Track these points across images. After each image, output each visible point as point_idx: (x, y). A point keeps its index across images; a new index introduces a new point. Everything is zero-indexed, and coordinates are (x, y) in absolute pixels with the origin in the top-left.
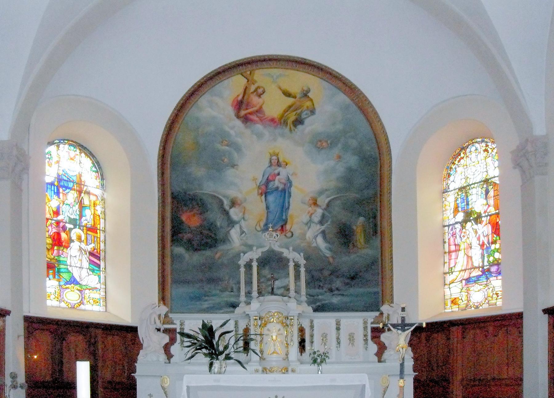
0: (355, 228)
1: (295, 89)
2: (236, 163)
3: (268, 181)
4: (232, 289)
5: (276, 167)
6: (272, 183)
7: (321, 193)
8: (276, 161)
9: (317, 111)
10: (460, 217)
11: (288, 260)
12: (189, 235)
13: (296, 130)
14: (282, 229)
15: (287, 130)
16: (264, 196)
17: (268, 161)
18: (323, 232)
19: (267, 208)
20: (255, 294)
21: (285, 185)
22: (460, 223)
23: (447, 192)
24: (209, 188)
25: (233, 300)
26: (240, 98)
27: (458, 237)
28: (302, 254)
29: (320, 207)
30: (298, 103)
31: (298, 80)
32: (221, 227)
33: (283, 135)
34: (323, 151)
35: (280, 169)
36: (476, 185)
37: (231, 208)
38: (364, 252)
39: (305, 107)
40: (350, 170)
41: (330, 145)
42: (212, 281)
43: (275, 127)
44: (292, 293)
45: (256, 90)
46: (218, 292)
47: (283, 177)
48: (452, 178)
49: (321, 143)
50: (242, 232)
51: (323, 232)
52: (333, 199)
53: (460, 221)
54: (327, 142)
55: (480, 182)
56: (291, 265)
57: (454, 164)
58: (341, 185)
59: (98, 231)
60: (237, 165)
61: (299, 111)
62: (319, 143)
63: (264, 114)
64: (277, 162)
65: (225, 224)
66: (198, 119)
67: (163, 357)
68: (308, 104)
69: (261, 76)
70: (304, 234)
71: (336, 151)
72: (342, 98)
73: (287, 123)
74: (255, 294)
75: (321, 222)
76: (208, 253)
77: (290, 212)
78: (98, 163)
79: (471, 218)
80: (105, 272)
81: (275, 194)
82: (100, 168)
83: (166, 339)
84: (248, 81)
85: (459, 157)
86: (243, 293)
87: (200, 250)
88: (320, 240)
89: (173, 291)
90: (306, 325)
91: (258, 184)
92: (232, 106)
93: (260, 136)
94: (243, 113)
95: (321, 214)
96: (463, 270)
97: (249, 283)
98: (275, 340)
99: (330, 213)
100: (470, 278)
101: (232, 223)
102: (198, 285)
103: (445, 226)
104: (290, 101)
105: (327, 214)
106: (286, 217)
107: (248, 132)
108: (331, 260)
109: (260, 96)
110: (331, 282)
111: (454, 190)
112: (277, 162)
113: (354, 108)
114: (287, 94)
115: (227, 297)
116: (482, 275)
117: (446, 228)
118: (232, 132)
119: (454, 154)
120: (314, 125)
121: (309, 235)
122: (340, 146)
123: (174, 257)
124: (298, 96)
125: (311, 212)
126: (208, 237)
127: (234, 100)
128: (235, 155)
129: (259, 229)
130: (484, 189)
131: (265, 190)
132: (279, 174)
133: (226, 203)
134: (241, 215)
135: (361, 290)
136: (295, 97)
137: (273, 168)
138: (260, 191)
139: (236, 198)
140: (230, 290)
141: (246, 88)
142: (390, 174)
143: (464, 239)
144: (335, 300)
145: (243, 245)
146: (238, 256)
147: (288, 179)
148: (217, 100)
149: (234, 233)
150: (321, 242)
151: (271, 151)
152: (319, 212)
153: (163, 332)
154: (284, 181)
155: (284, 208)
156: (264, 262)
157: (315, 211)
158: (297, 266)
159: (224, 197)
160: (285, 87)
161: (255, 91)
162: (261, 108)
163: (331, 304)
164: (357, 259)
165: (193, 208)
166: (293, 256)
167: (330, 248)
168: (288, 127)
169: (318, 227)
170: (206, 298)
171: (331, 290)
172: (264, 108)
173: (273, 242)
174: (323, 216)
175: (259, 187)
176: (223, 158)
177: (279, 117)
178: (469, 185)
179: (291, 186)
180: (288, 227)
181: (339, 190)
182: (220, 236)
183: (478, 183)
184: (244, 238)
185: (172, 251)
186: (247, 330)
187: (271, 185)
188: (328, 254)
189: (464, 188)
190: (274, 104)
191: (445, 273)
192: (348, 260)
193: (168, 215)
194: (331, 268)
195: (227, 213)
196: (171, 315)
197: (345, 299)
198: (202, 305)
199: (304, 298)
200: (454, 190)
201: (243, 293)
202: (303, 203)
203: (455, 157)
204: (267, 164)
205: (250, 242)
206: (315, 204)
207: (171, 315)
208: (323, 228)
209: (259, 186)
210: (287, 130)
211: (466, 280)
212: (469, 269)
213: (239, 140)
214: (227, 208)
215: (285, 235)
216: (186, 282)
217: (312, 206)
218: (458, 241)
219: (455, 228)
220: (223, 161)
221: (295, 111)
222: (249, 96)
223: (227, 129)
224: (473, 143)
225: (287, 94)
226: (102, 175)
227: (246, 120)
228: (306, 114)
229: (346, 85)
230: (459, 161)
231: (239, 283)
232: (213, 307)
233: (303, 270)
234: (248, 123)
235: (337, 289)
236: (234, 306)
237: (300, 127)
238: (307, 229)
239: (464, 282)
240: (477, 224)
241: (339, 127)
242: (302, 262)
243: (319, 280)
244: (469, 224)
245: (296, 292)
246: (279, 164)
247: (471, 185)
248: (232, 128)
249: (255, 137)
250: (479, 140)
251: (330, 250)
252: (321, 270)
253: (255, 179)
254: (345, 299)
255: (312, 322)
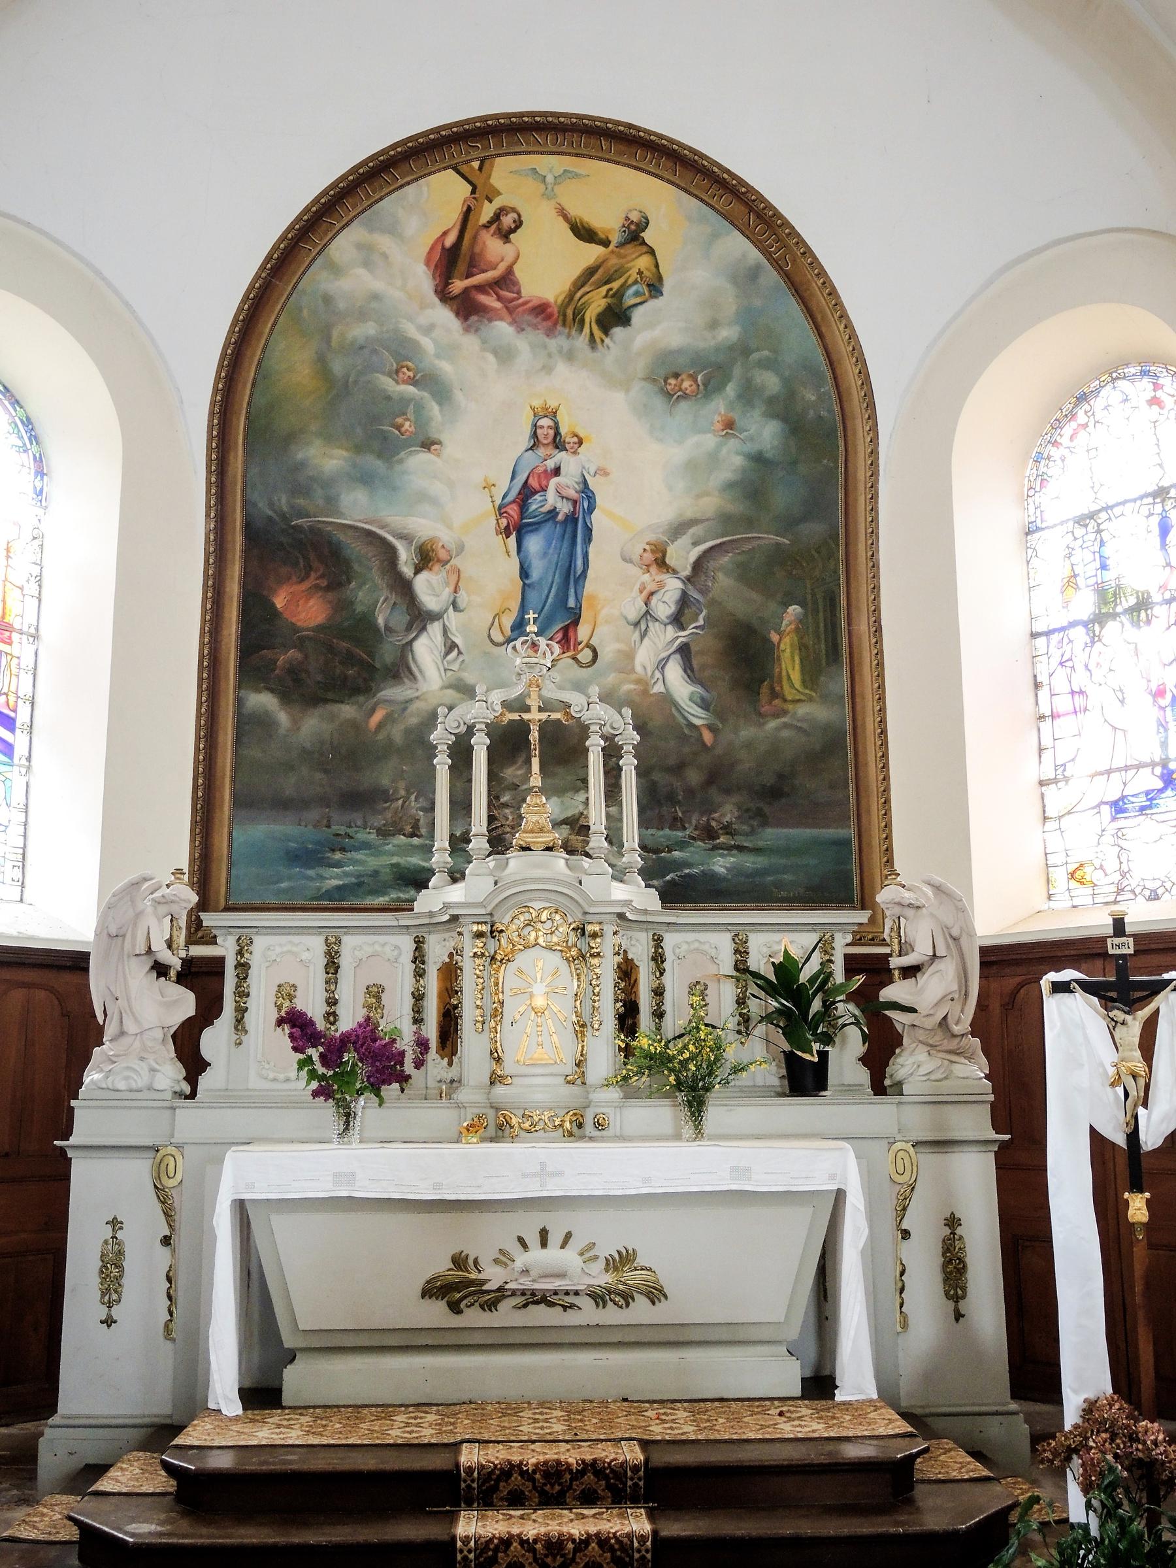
0: (775, 637)
1: (608, 221)
2: (434, 435)
3: (526, 493)
4: (416, 826)
5: (550, 450)
6: (537, 497)
7: (678, 529)
8: (552, 432)
9: (666, 289)
10: (1085, 604)
11: (584, 730)
12: (293, 654)
13: (607, 341)
14: (567, 639)
15: (582, 341)
16: (513, 537)
17: (528, 430)
18: (684, 651)
19: (524, 573)
20: (479, 844)
21: (575, 502)
22: (1085, 624)
23: (1038, 529)
24: (356, 508)
25: (415, 860)
26: (450, 241)
27: (1079, 667)
28: (627, 712)
29: (675, 572)
30: (614, 261)
31: (614, 192)
32: (387, 628)
33: (570, 356)
34: (684, 405)
35: (561, 457)
36: (1129, 506)
37: (418, 571)
38: (807, 710)
39: (633, 274)
40: (758, 459)
41: (701, 387)
42: (360, 800)
43: (550, 333)
44: (597, 842)
45: (497, 217)
46: (372, 837)
47: (568, 481)
48: (1051, 488)
49: (680, 380)
50: (451, 647)
51: (684, 651)
52: (712, 548)
53: (1085, 618)
54: (694, 378)
55: (1141, 498)
56: (595, 744)
57: (1056, 444)
58: (735, 508)
59: (15, 636)
60: (439, 443)
61: (615, 285)
62: (672, 381)
63: (519, 292)
64: (551, 437)
65: (400, 619)
66: (327, 300)
67: (171, 1073)
68: (644, 262)
69: (513, 176)
70: (630, 656)
71: (718, 407)
72: (737, 247)
73: (582, 321)
74: (479, 844)
75: (678, 620)
76: (347, 711)
77: (590, 587)
78: (28, 422)
79: (1119, 609)
80: (29, 768)
81: (547, 528)
82: (35, 438)
83: (185, 1004)
84: (473, 192)
85: (1073, 424)
86: (442, 840)
87: (326, 701)
88: (674, 672)
89: (247, 835)
90: (640, 952)
91: (498, 502)
92: (427, 263)
93: (504, 355)
94: (458, 285)
95: (677, 595)
96: (1102, 774)
97: (461, 805)
98: (540, 1012)
99: (704, 591)
100: (1123, 798)
101: (420, 618)
102: (314, 814)
103: (1034, 635)
104: (592, 253)
105: (694, 594)
106: (578, 600)
107: (470, 342)
108: (708, 737)
109: (505, 235)
110: (709, 808)
111: (1062, 523)
112: (551, 437)
113: (771, 276)
114: (584, 233)
115: (396, 853)
116: (1161, 791)
117: (1041, 642)
118: (427, 343)
119: (1058, 415)
120: (658, 327)
121: (645, 656)
122: (731, 390)
123: (251, 726)
124: (615, 239)
125: (651, 587)
126: (349, 659)
127: (432, 248)
128: (434, 409)
129: (499, 638)
130: (1155, 520)
131: (519, 517)
132: (557, 471)
133: (405, 557)
134: (447, 593)
135: (807, 833)
136: (605, 243)
137: (541, 452)
138: (504, 522)
139: (433, 540)
140: (408, 829)
141: (469, 209)
142: (875, 474)
143: (1098, 675)
144: (721, 864)
145: (450, 687)
146: (431, 720)
147: (585, 488)
148: (384, 242)
149: (426, 650)
150: (678, 685)
151: (537, 403)
152: (673, 586)
153: (178, 982)
154: (572, 494)
155: (572, 576)
156: (509, 742)
157: (661, 585)
158: (612, 752)
159: (401, 537)
160: (577, 211)
161: (491, 223)
162: (510, 271)
163: (710, 876)
164: (785, 734)
165: (309, 568)
166: (605, 720)
167: (702, 699)
168: (586, 330)
169: (671, 631)
170: (338, 856)
171: (709, 834)
172: (519, 273)
173: (536, 678)
174: (684, 601)
175: (501, 511)
176: (399, 420)
177: (560, 301)
178: (1106, 509)
179: (591, 509)
180: (583, 632)
181: (727, 521)
182: (387, 654)
183: (1135, 500)
184: (455, 667)
185: (240, 702)
186: (451, 972)
187: (535, 504)
188: (698, 716)
189: (1092, 516)
190: (546, 264)
191: (1042, 783)
192: (758, 735)
193: (233, 589)
194: (705, 759)
195: (404, 588)
196: (209, 919)
197: (750, 862)
198: (322, 878)
199: (633, 858)
200: (1062, 523)
201: (442, 840)
202: (627, 560)
203: (1057, 425)
204: (525, 441)
205: (469, 677)
206: (661, 563)
207: (209, 919)
208: (683, 636)
209: (500, 508)
210: (582, 341)
211: (1115, 803)
212: (1119, 770)
213: (445, 367)
214: (407, 570)
215: (574, 658)
216: (282, 805)
217: (654, 569)
218: (1080, 680)
219: (1071, 641)
220: (399, 427)
221: (607, 283)
222: (475, 238)
223: (412, 331)
224: (1114, 380)
225: (584, 233)
226: (39, 460)
227: (467, 308)
228: (637, 294)
229: (751, 210)
230: (1072, 438)
231: (431, 808)
232: (360, 885)
233: (629, 764)
234: (474, 318)
235: (728, 829)
236: (419, 880)
237: (618, 331)
238: (634, 651)
239: (1106, 810)
240: (1136, 624)
241: (729, 334)
242: (630, 738)
243: (671, 798)
244: (1112, 626)
245: (608, 838)
246: (558, 443)
247: (1112, 507)
248: (428, 330)
249: (491, 358)
250: (1132, 370)
251: (705, 705)
252: (679, 769)
253: (488, 486)
254: (750, 862)
255: (658, 941)
